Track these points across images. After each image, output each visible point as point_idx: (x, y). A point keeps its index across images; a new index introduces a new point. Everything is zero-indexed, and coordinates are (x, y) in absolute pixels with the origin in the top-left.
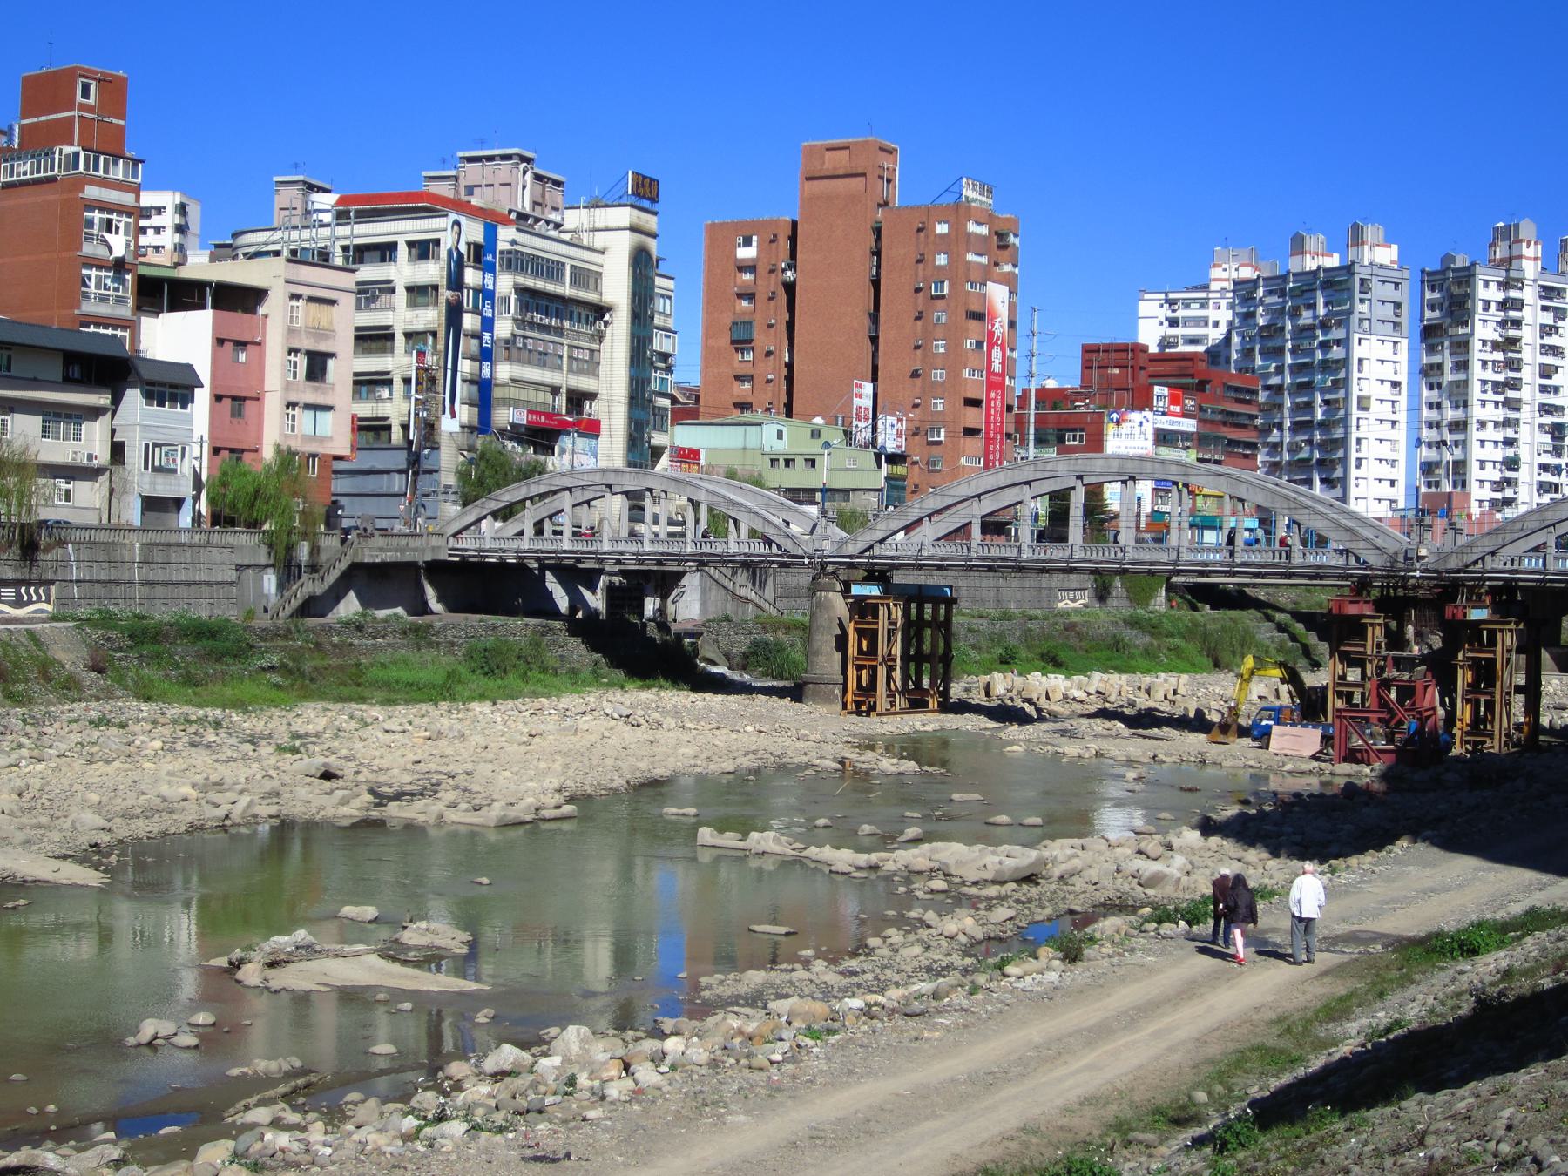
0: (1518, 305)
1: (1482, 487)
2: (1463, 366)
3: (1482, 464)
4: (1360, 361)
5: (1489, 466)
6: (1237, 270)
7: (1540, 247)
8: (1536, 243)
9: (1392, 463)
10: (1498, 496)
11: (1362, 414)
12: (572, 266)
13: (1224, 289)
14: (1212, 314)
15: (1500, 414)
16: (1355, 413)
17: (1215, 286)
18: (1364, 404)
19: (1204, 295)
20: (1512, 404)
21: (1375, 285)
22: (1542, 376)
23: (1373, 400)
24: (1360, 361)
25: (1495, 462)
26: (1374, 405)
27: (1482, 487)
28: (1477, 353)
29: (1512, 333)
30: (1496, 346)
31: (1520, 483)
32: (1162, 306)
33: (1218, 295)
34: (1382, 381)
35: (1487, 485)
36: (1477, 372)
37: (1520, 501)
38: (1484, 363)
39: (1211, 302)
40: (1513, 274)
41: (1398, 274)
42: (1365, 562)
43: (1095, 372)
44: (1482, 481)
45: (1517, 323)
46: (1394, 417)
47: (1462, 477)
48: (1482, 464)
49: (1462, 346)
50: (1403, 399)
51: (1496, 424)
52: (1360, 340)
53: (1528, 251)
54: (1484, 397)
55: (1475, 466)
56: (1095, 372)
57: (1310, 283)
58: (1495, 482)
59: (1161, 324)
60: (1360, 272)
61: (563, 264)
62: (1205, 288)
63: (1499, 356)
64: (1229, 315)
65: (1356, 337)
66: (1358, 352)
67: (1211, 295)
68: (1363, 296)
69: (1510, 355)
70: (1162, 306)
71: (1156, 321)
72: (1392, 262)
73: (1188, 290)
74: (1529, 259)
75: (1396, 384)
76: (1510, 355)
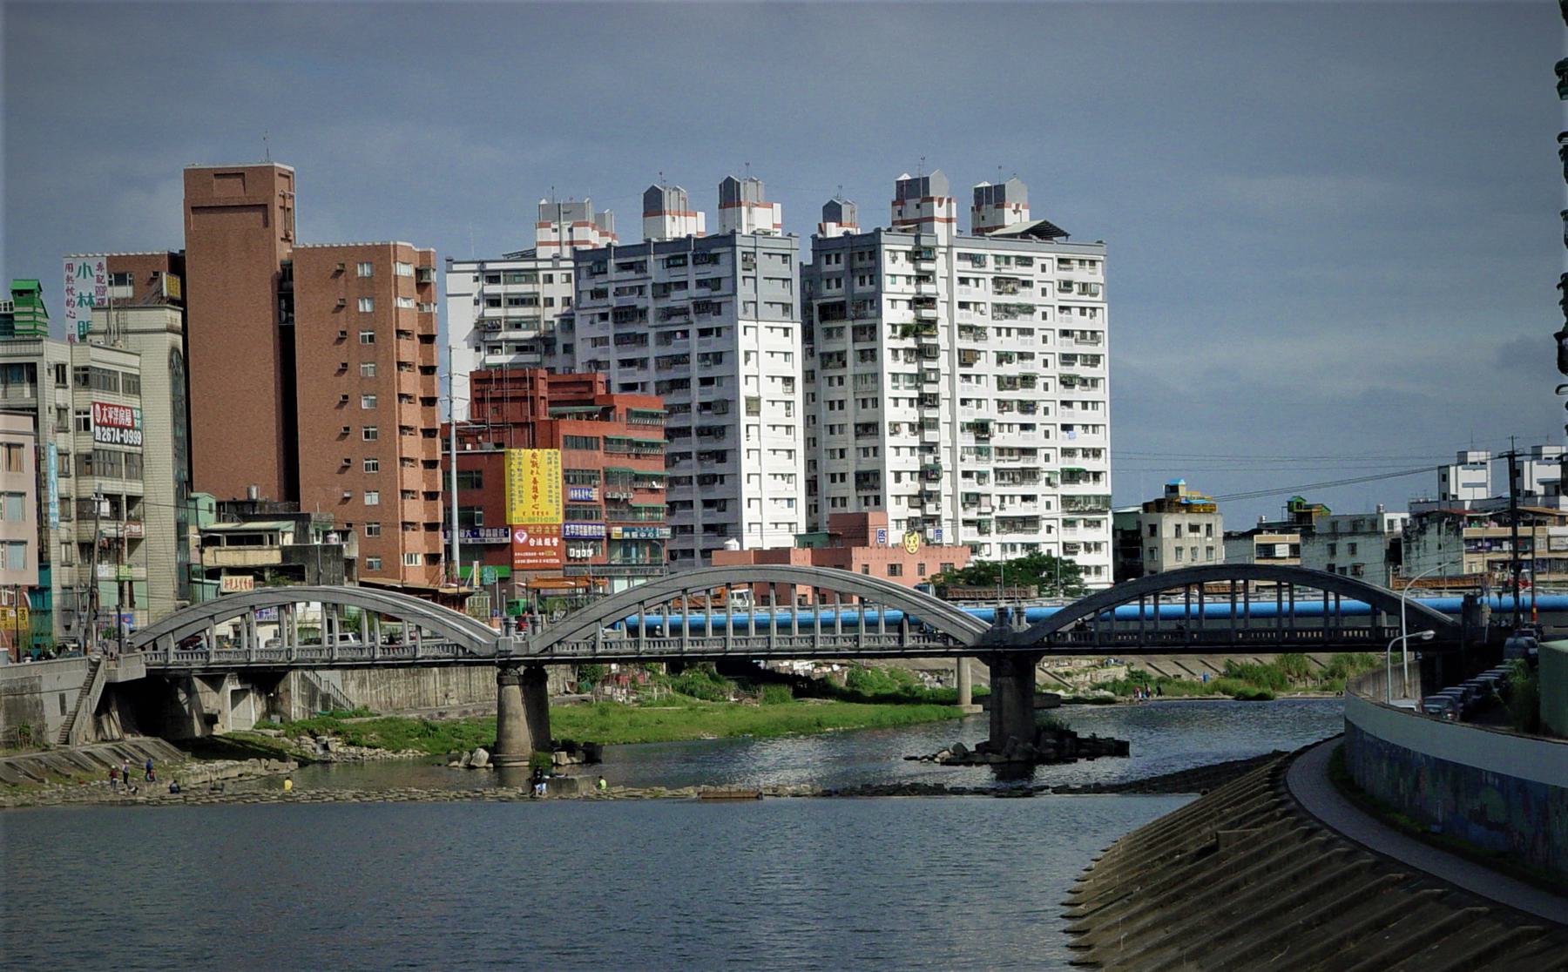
0: (933, 496)
1: (898, 503)
2: (871, 355)
3: (898, 476)
4: (747, 353)
5: (905, 477)
6: (571, 230)
7: (954, 205)
8: (949, 201)
9: (787, 477)
10: (917, 513)
11: (753, 420)
12: (123, 373)
13: (557, 258)
14: (544, 290)
15: (913, 415)
16: (745, 419)
17: (542, 252)
18: (754, 405)
19: (531, 265)
20: (923, 353)
21: (761, 259)
22: (962, 364)
23: (763, 402)
24: (747, 353)
25: (912, 472)
26: (764, 405)
27: (898, 503)
28: (888, 342)
29: (926, 313)
30: (906, 331)
31: (943, 498)
32: (477, 279)
33: (549, 265)
34: (773, 378)
35: (904, 500)
36: (889, 365)
37: (943, 518)
38: (895, 351)
39: (541, 274)
40: (925, 241)
41: (787, 244)
42: (470, 652)
43: (489, 407)
44: (898, 497)
45: (934, 424)
46: (788, 421)
47: (874, 493)
48: (898, 476)
49: (872, 331)
50: (798, 397)
51: (911, 426)
52: (745, 327)
53: (940, 212)
54: (896, 394)
55: (889, 478)
56: (489, 407)
57: (677, 252)
58: (910, 497)
59: (476, 302)
60: (743, 244)
61: (116, 372)
62: (530, 255)
63: (910, 342)
64: (569, 290)
65: (741, 324)
66: (745, 342)
67: (540, 265)
68: (747, 273)
69: (925, 341)
70: (477, 279)
71: (471, 300)
72: (775, 226)
73: (509, 258)
74: (940, 220)
75: (788, 380)
76: (925, 341)
